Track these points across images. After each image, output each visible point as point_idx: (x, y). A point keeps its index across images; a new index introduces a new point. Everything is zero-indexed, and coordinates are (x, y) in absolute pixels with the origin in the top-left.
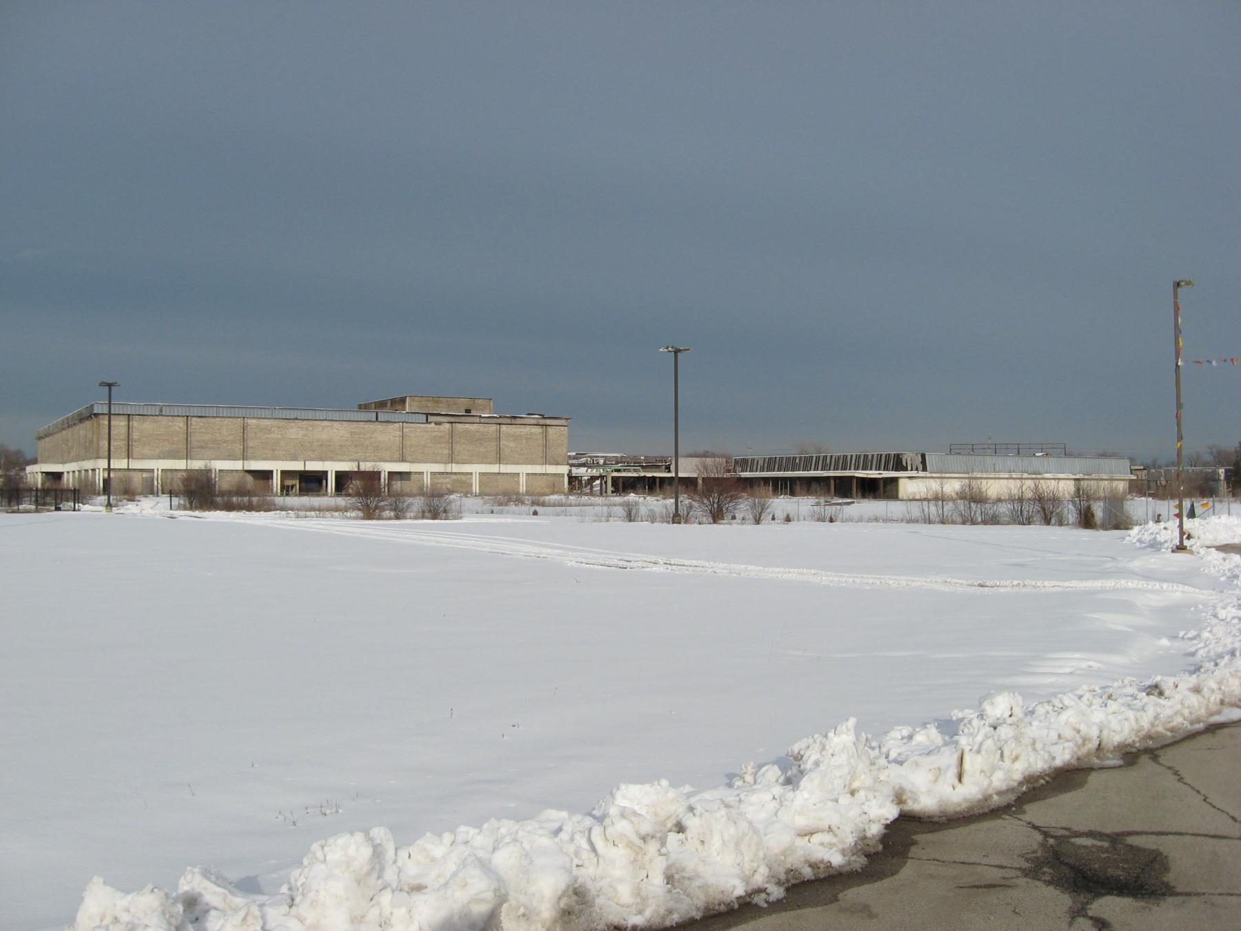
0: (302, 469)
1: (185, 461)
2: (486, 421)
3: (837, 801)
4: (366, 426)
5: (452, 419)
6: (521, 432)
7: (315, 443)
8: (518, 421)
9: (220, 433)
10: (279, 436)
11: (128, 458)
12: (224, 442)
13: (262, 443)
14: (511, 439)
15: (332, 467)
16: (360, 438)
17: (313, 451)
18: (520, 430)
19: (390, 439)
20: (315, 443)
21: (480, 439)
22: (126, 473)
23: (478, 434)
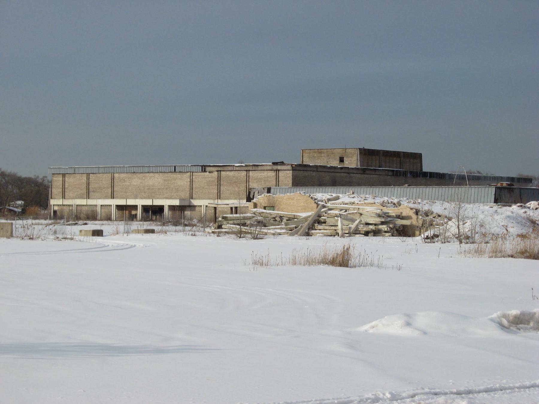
0: (151, 204)
1: (86, 199)
2: (237, 169)
3: (84, 391)
4: (172, 176)
5: (219, 169)
6: (261, 176)
7: (146, 188)
8: (260, 168)
9: (102, 183)
10: (129, 184)
11: (63, 199)
12: (104, 188)
13: (121, 188)
14: (255, 181)
15: (140, 202)
16: (168, 183)
17: (145, 192)
18: (260, 174)
19: (184, 183)
20: (146, 188)
21: (235, 182)
22: (62, 207)
23: (234, 178)
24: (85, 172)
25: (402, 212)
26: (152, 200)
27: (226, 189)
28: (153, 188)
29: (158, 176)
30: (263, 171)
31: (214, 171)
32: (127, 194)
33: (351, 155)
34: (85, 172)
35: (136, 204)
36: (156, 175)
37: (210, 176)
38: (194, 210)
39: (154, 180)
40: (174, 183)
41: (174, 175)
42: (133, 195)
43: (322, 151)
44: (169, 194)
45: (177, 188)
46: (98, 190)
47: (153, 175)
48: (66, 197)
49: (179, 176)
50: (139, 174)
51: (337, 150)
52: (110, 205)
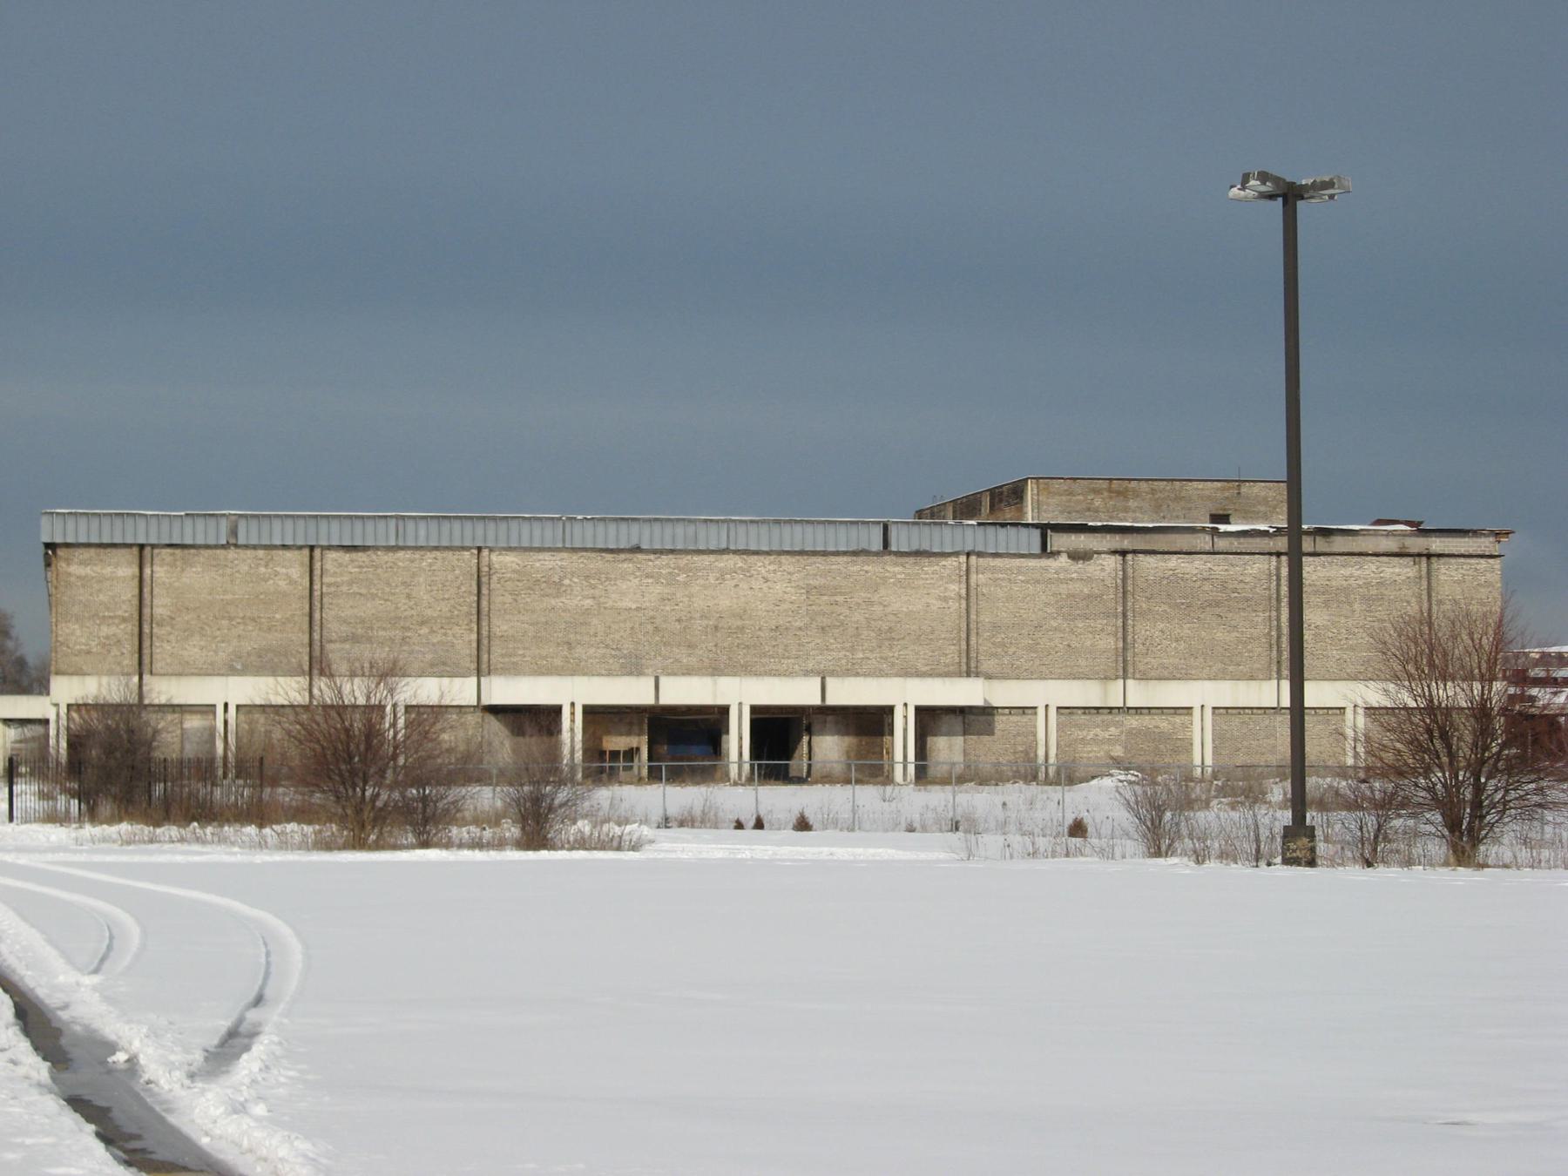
4: (856, 568)
5: (1126, 542)
7: (698, 624)
8: (1339, 544)
9: (409, 596)
10: (588, 602)
12: (423, 623)
17: (691, 646)
20: (698, 624)
23: (1207, 587)
24: (618, 539)
25: (996, 737)
26: (819, 679)
27: (1162, 631)
28: (739, 623)
29: (772, 568)
30: (1356, 559)
31: (1099, 553)
32: (579, 652)
33: (1262, 508)
34: (618, 539)
35: (720, 702)
36: (761, 565)
37: (1074, 575)
38: (990, 731)
39: (743, 585)
40: (871, 603)
41: (866, 568)
42: (614, 657)
43: (1126, 488)
44: (841, 654)
45: (885, 627)
46: (381, 633)
47: (740, 564)
48: (157, 666)
49: (897, 569)
50: (652, 557)
51: (1201, 485)
52: (1023, 710)
